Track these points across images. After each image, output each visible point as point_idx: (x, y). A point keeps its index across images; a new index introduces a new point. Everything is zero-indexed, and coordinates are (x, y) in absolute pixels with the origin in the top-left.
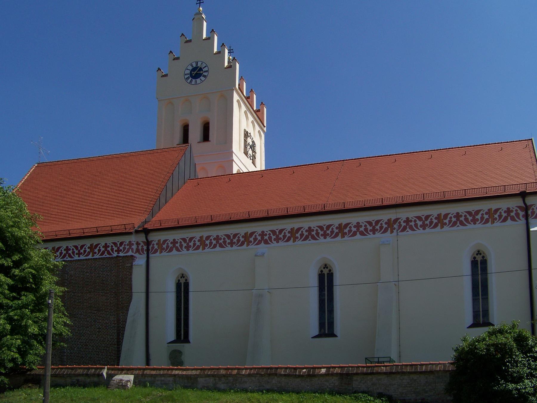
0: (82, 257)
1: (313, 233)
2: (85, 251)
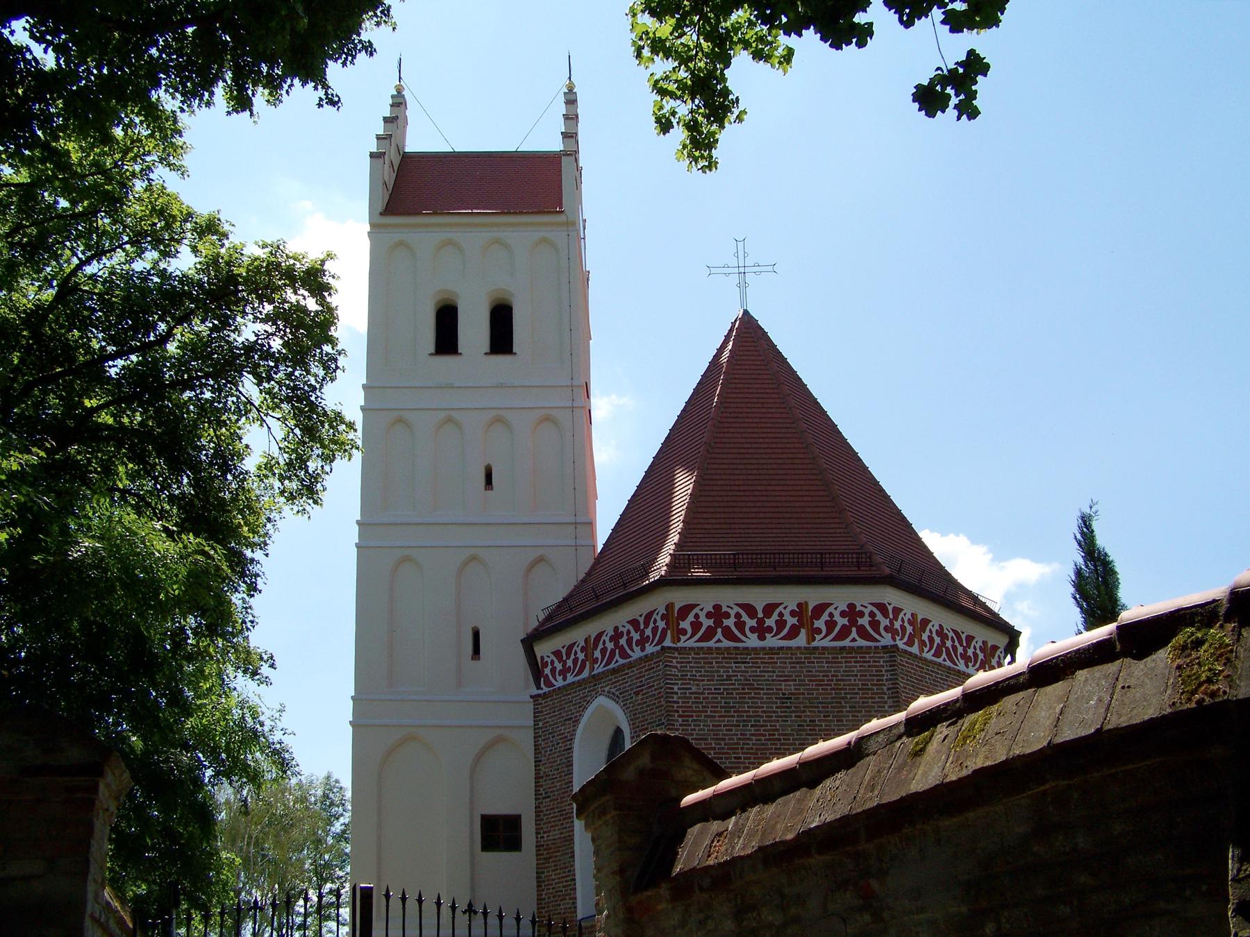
0: (772, 641)
2: (781, 623)
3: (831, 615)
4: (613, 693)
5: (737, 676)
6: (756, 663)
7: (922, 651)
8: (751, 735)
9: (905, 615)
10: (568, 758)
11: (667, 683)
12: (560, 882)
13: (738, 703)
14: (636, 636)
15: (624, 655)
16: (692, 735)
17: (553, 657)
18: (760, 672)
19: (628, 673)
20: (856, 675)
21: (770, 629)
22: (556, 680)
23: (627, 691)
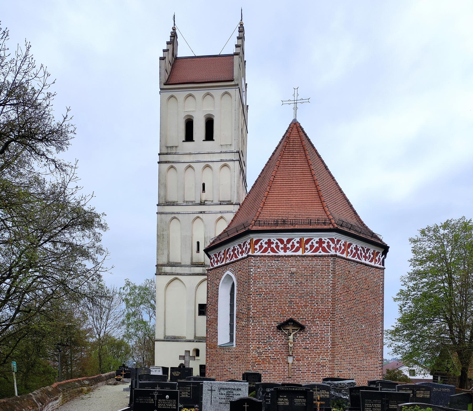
0: (289, 253)
2: (293, 246)
5: (275, 265)
9: (342, 242)
11: (249, 268)
15: (236, 257)
17: (214, 256)
21: (288, 248)
23: (236, 270)
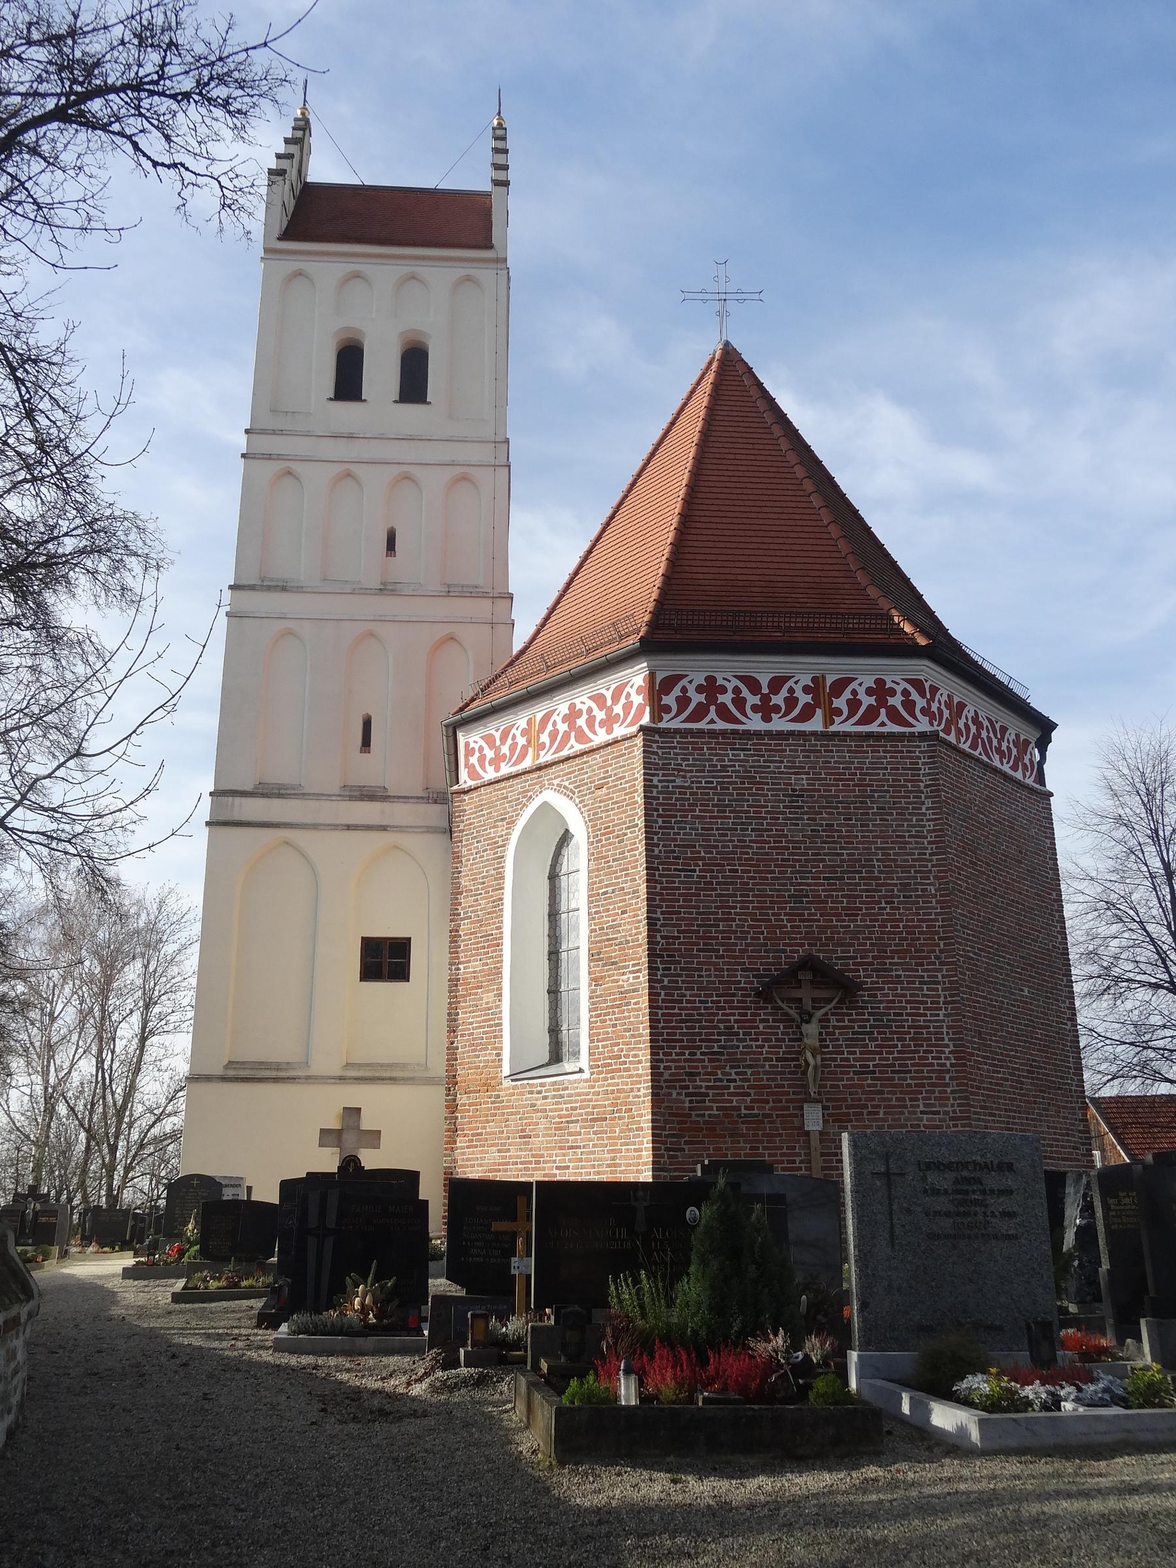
0: (779, 724)
1: (891, 701)
2: (791, 701)
3: (854, 693)
4: (565, 787)
5: (735, 766)
6: (760, 750)
7: (959, 741)
8: (750, 841)
9: (941, 695)
10: (498, 868)
12: (480, 1027)
13: (735, 800)
14: (600, 715)
15: (581, 737)
16: (676, 840)
17: (482, 743)
18: (765, 761)
19: (588, 762)
20: (886, 769)
21: (777, 709)
22: (485, 771)
